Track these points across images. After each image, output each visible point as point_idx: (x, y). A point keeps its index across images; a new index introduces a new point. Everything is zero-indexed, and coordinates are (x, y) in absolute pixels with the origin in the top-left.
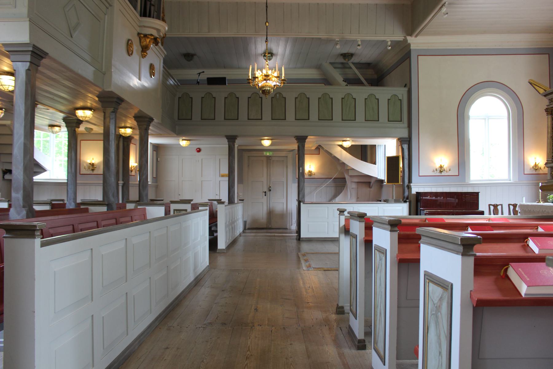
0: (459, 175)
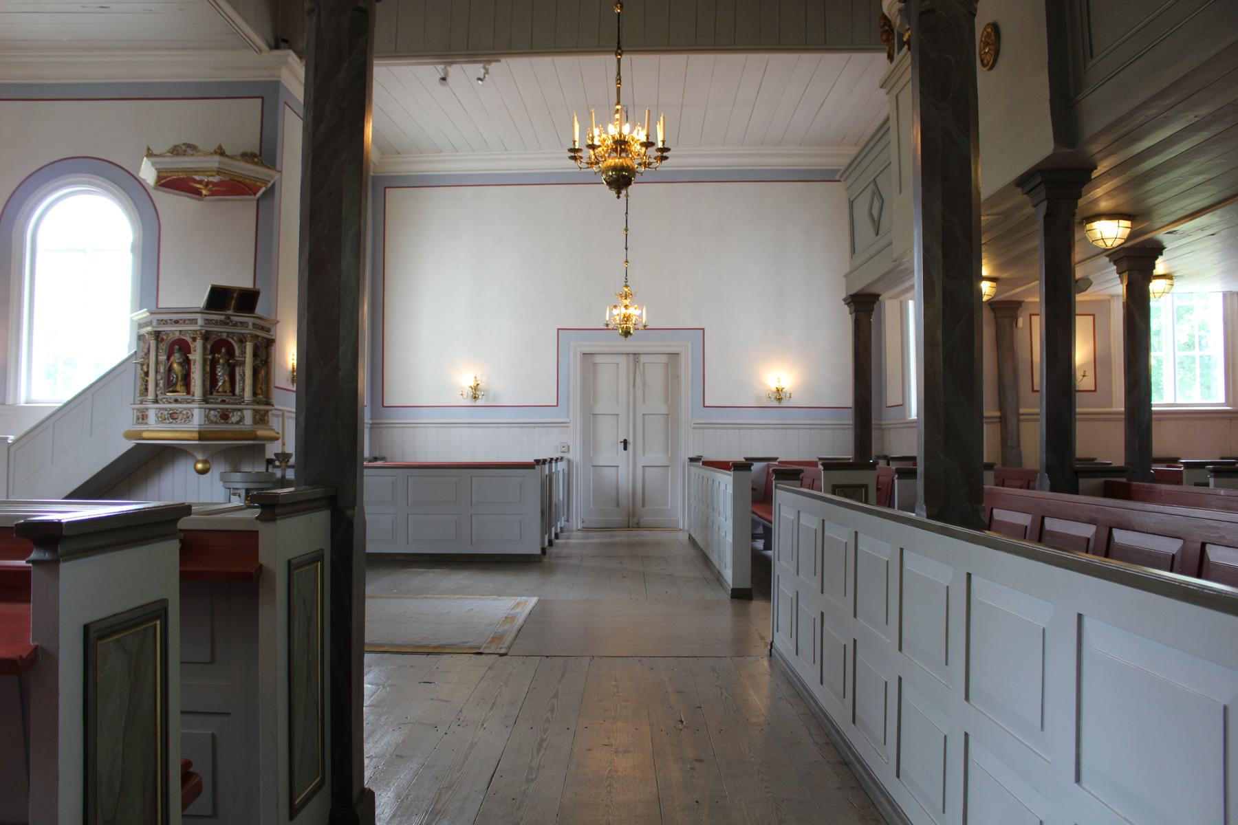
0: (704, 407)
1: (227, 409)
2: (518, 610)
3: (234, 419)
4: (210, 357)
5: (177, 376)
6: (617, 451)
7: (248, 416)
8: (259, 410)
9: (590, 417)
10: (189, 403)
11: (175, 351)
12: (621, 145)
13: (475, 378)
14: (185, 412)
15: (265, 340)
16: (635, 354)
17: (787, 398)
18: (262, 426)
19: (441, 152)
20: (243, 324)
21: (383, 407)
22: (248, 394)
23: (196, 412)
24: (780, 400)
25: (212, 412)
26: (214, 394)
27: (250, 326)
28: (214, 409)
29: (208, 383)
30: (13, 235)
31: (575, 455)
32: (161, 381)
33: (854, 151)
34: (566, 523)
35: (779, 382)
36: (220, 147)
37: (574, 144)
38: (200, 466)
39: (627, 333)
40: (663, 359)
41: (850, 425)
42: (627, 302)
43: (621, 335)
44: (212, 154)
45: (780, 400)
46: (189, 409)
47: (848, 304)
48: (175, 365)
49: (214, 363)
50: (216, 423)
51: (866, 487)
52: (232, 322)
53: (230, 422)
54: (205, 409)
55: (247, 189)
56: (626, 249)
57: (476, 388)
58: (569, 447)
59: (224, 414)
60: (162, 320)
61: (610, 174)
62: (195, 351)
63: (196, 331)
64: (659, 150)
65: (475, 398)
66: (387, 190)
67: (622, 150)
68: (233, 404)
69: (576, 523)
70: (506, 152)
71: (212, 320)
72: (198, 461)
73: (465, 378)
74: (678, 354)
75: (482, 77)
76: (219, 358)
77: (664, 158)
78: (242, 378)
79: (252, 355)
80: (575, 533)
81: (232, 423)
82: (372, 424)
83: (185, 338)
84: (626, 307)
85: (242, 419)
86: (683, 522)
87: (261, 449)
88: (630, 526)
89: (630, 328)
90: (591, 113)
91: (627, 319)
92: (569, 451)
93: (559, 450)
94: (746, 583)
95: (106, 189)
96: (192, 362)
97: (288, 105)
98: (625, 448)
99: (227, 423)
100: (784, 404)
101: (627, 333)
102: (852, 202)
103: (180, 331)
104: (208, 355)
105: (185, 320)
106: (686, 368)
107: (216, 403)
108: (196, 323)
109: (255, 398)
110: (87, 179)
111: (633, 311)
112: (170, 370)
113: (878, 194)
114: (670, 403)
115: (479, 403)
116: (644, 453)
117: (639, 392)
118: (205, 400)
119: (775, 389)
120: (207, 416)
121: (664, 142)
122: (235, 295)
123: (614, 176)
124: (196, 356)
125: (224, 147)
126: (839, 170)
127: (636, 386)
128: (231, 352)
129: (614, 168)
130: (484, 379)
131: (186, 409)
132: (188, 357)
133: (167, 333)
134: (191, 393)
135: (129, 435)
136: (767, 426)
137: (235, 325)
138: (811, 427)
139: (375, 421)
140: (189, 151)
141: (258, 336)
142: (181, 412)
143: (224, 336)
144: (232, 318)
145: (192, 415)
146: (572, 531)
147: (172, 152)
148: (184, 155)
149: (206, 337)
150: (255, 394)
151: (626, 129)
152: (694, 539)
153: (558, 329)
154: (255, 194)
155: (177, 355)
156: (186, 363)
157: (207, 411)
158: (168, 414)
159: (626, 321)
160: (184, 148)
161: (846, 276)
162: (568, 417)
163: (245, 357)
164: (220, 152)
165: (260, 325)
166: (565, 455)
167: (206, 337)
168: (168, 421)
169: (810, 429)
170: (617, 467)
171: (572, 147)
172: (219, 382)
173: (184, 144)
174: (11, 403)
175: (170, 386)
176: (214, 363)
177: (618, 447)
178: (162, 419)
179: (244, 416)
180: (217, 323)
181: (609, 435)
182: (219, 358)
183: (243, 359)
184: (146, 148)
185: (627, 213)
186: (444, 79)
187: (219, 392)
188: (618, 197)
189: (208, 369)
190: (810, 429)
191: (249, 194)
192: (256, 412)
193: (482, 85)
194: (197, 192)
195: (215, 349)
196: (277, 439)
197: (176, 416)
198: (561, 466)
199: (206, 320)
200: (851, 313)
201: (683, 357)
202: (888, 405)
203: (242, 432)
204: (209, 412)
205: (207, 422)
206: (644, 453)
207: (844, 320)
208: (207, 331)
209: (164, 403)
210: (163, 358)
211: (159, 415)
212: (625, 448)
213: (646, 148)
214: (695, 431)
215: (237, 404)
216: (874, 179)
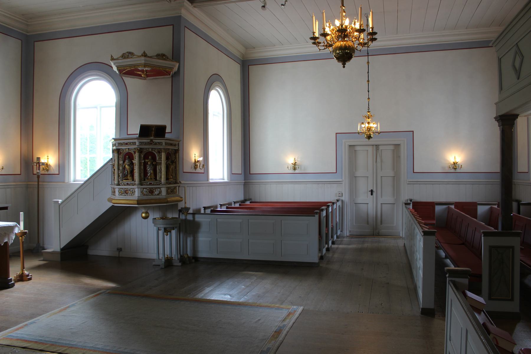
0: (414, 172)
1: (152, 188)
2: (285, 323)
3: (157, 192)
4: (143, 161)
5: (127, 171)
6: (368, 195)
7: (164, 191)
8: (169, 187)
9: (353, 178)
10: (133, 185)
11: (127, 159)
12: (342, 32)
13: (295, 159)
14: (131, 190)
15: (174, 150)
16: (376, 145)
17: (460, 168)
18: (172, 195)
19: (275, 46)
20: (160, 144)
21: (250, 174)
22: (163, 180)
23: (136, 190)
24: (455, 169)
25: (145, 190)
26: (146, 180)
27: (164, 144)
28: (146, 188)
29: (142, 175)
30: (66, 102)
31: (346, 198)
32: (121, 174)
33: (501, 29)
34: (341, 232)
35: (455, 159)
36: (144, 52)
37: (314, 34)
38: (144, 215)
39: (369, 137)
40: (392, 147)
41: (498, 182)
42: (369, 120)
43: (366, 138)
44: (140, 56)
45: (455, 169)
46: (160, 188)
47: (498, 121)
48: (126, 166)
49: (145, 164)
50: (147, 195)
51: (513, 248)
52: (154, 142)
53: (154, 194)
54: (141, 188)
55: (165, 72)
56: (368, 91)
57: (295, 164)
58: (342, 194)
59: (151, 190)
60: (120, 143)
61: (338, 52)
62: (135, 158)
63: (135, 148)
64: (370, 34)
65: (295, 169)
66: (249, 66)
67: (346, 36)
68: (155, 185)
69: (346, 233)
70: (307, 44)
71: (143, 142)
72: (143, 213)
73: (290, 160)
74: (400, 145)
75: (284, 3)
76: (148, 162)
77: (374, 40)
78: (160, 171)
79: (165, 159)
80: (345, 239)
81: (155, 195)
82: (245, 183)
83: (131, 152)
84: (369, 123)
85: (160, 192)
86: (402, 234)
87: (177, 205)
88: (374, 234)
89: (371, 134)
90: (323, 13)
91: (369, 129)
92: (342, 196)
93: (337, 195)
94: (431, 305)
95: (103, 77)
96: (134, 164)
97: (186, 27)
98: (372, 194)
99: (152, 195)
100: (458, 171)
101: (369, 137)
102: (500, 59)
103: (129, 149)
104: (143, 160)
105: (130, 143)
106: (404, 151)
107: (148, 185)
108: (136, 144)
109: (167, 181)
110: (95, 73)
111: (373, 125)
112: (124, 168)
113: (519, 52)
114: (395, 171)
115: (297, 171)
116: (382, 197)
117: (379, 165)
118: (141, 184)
119: (452, 163)
120: (142, 192)
121: (372, 28)
122: (154, 129)
123: (340, 53)
124: (136, 161)
125: (146, 52)
126: (492, 40)
127: (377, 162)
128: (154, 158)
129: (340, 48)
130: (299, 160)
131: (132, 188)
132: (132, 162)
133: (123, 150)
134: (134, 180)
135: (110, 200)
136: (448, 183)
137: (156, 144)
138: (473, 183)
139: (246, 181)
140: (130, 56)
141: (169, 149)
142: (130, 190)
143: (150, 150)
144: (154, 140)
145: (135, 191)
146: (344, 237)
147: (122, 57)
148: (128, 58)
149: (140, 151)
150: (167, 179)
151: (347, 22)
152: (405, 247)
153: (336, 133)
154: (170, 75)
155: (127, 161)
156: (132, 164)
157: (142, 189)
158: (124, 191)
159: (369, 131)
160: (127, 54)
161: (496, 104)
162: (342, 178)
163: (161, 160)
164: (145, 55)
165: (169, 143)
166: (341, 198)
167: (140, 151)
168: (124, 195)
169: (473, 184)
170: (368, 204)
171: (312, 36)
172: (148, 174)
173: (127, 52)
174: (67, 182)
175: (125, 177)
176: (145, 164)
177: (368, 194)
178: (121, 193)
179: (161, 191)
180: (146, 144)
181: (363, 187)
182: (148, 162)
183: (161, 161)
184: (111, 56)
185: (368, 72)
186: (264, 7)
187: (148, 179)
188: (344, 67)
189: (142, 167)
190: (473, 184)
191: (167, 75)
192: (168, 188)
193: (284, 8)
194: (140, 75)
195: (146, 157)
196: (182, 201)
197: (127, 192)
198: (339, 203)
199: (140, 142)
200: (499, 126)
201: (402, 147)
202: (518, 171)
203: (160, 199)
204: (143, 190)
205: (142, 195)
206: (382, 197)
207: (496, 130)
208: (141, 148)
209: (122, 185)
210: (121, 162)
211: (120, 191)
212: (372, 194)
213: (360, 33)
214: (409, 185)
215: (158, 185)
216: (517, 44)
